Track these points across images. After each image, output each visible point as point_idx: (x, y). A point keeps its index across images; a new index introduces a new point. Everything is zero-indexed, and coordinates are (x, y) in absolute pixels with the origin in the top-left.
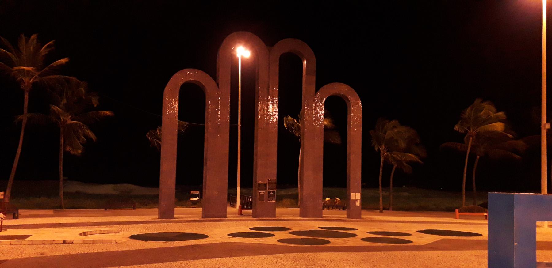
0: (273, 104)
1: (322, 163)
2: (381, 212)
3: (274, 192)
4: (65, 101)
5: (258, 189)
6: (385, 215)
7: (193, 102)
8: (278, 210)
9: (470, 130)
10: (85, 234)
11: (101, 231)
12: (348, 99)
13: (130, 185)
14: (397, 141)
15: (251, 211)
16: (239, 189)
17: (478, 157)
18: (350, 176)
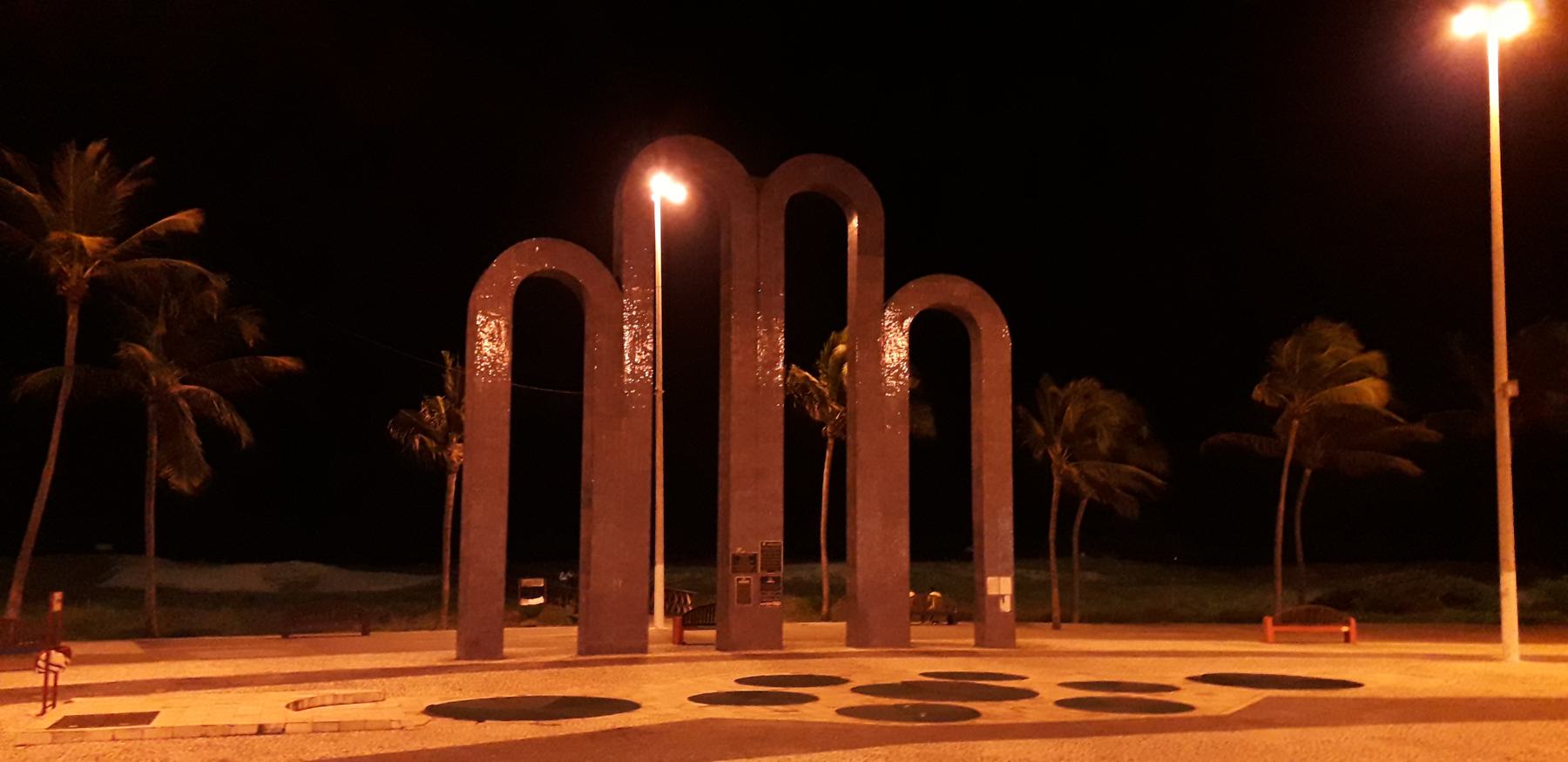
0: (770, 331)
1: (905, 494)
2: (1056, 627)
3: (777, 579)
4: (161, 329)
5: (735, 571)
7: (554, 334)
8: (788, 628)
10: (296, 706)
11: (336, 696)
12: (972, 320)
13: (312, 565)
15: (710, 634)
16: (1509, 580)
17: (1308, 472)
18: (981, 529)
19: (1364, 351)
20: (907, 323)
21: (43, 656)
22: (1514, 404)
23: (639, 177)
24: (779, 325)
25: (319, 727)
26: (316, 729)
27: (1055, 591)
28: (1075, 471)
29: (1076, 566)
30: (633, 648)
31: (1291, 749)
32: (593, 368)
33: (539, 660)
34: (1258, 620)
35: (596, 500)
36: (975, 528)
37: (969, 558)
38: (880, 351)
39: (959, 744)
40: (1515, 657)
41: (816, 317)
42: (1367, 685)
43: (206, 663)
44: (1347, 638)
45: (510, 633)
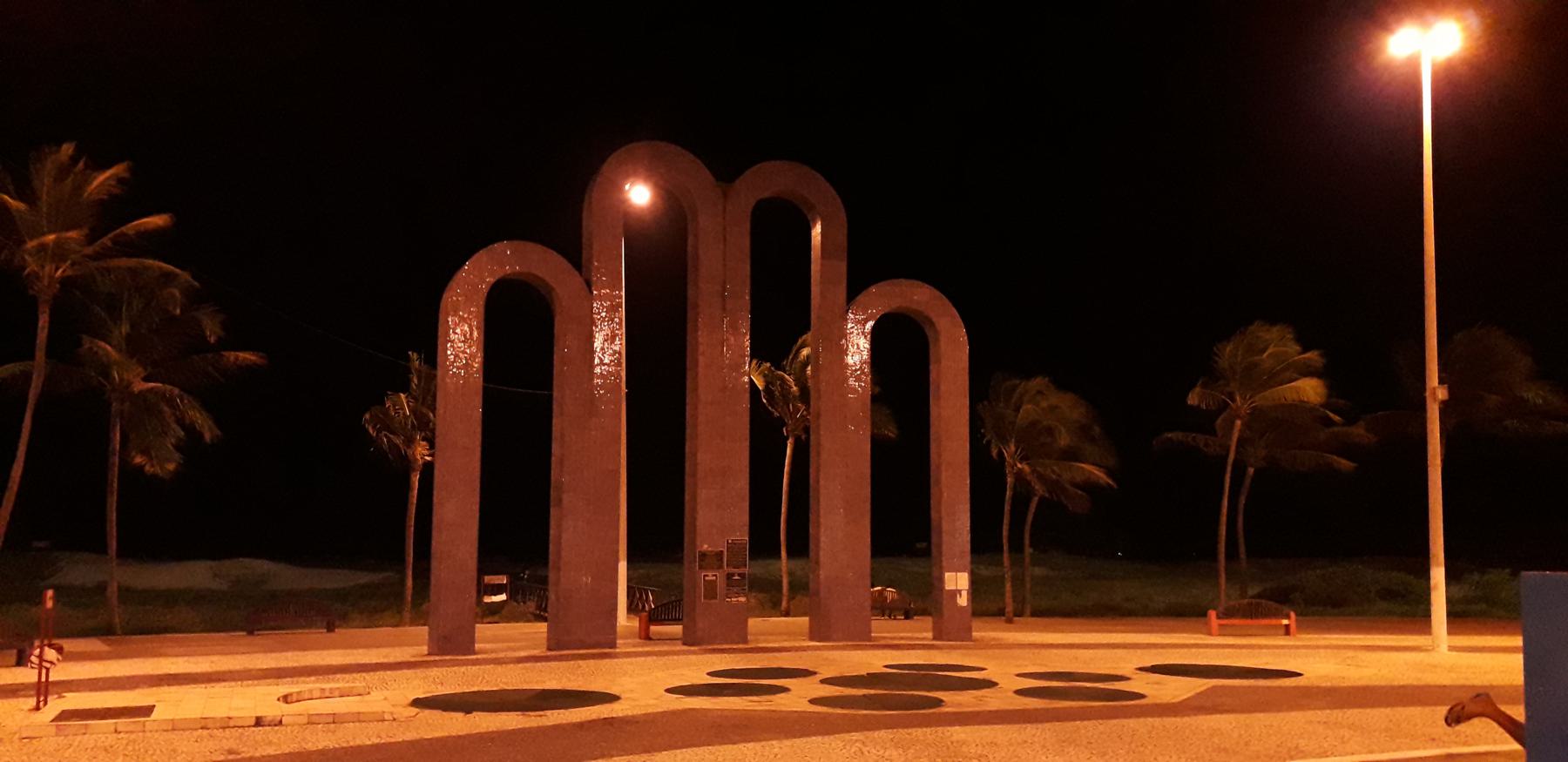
1: (866, 491)
2: (1010, 621)
4: (125, 328)
5: (701, 567)
6: (1020, 630)
9: (1234, 400)
10: (286, 699)
12: (932, 324)
14: (1050, 431)
15: (677, 629)
16: (1438, 575)
18: (940, 525)
19: (1305, 350)
20: (870, 325)
21: (37, 652)
22: (1445, 408)
23: (621, 189)
24: (745, 329)
25: (314, 719)
26: (312, 721)
27: (1008, 586)
28: (1027, 468)
29: (1027, 560)
30: (602, 642)
31: (1235, 735)
32: (561, 369)
33: (511, 653)
34: (1202, 614)
35: (566, 498)
36: (934, 524)
37: (927, 553)
38: (844, 352)
39: (928, 730)
40: (1444, 647)
41: (781, 322)
42: (1306, 675)
43: (180, 660)
44: (1287, 630)
45: (483, 630)
